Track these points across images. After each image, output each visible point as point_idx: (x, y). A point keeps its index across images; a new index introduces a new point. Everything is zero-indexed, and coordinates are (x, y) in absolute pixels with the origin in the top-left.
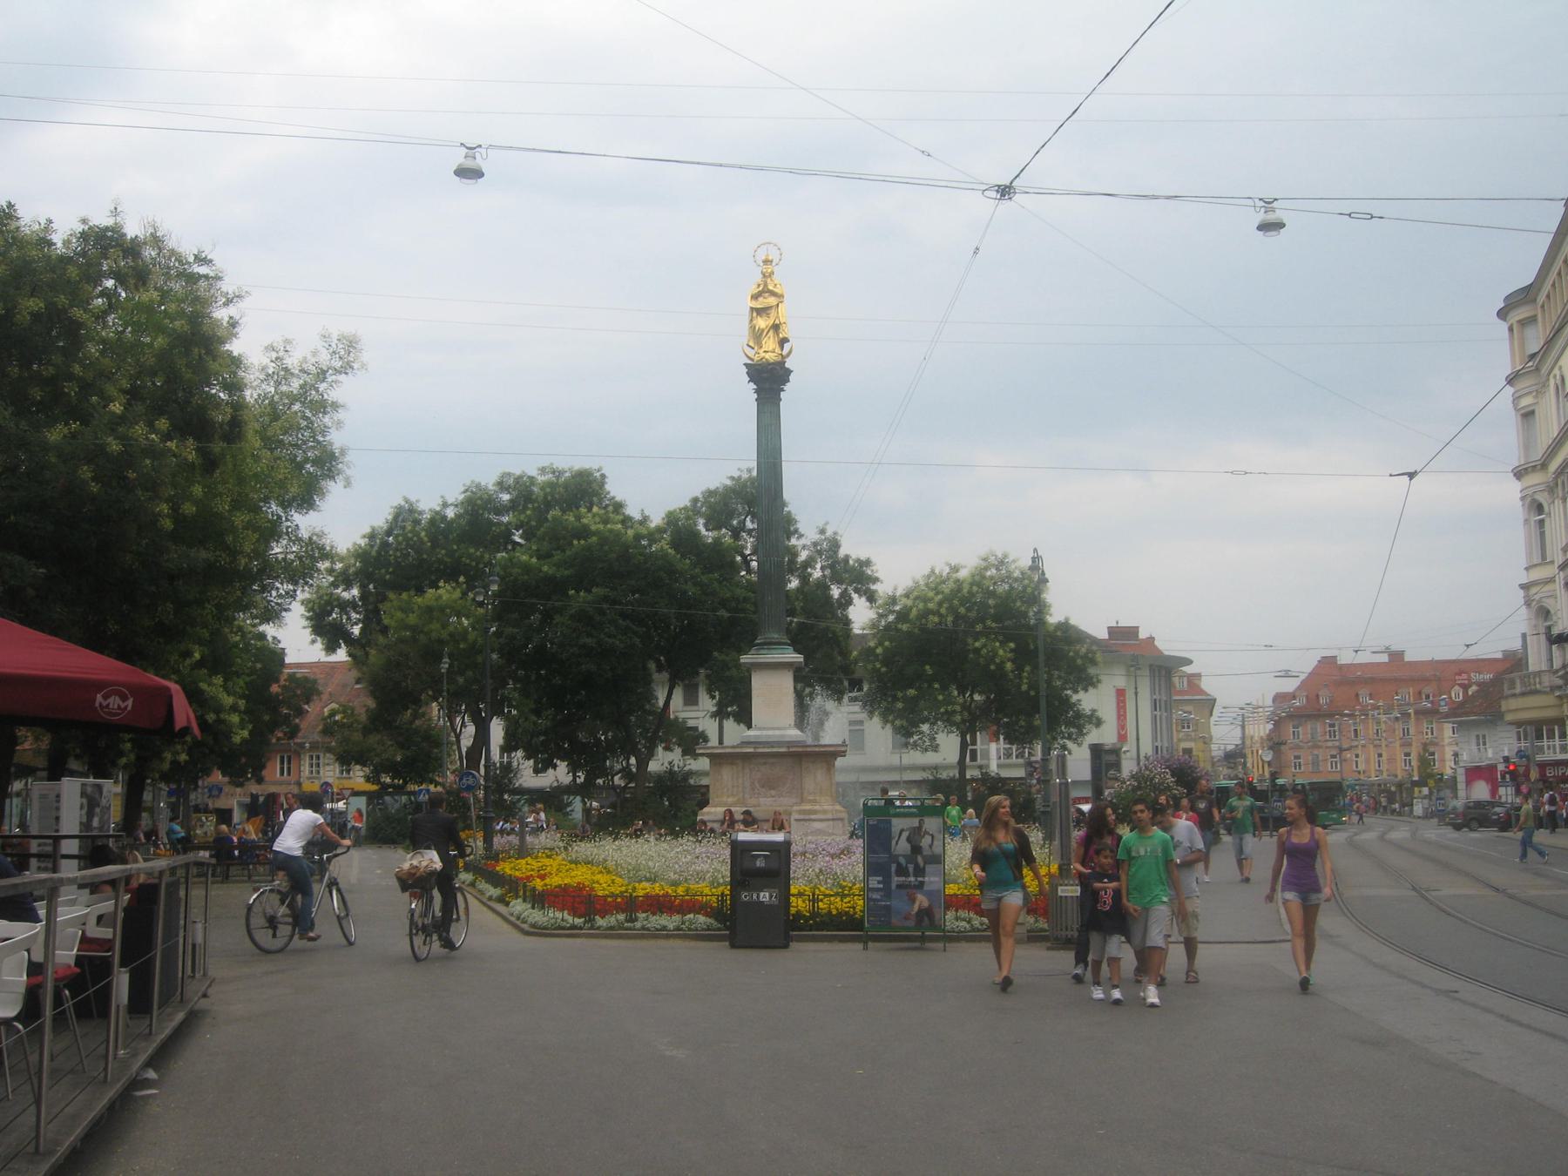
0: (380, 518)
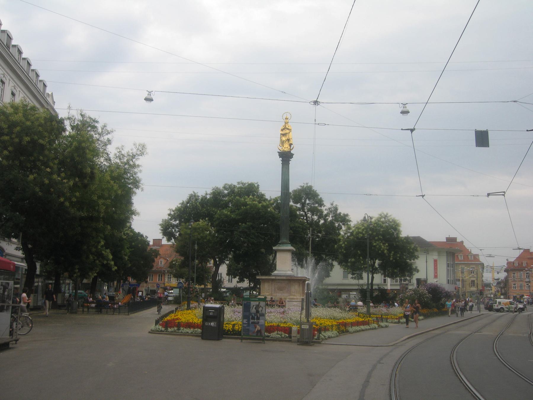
0: (185, 198)
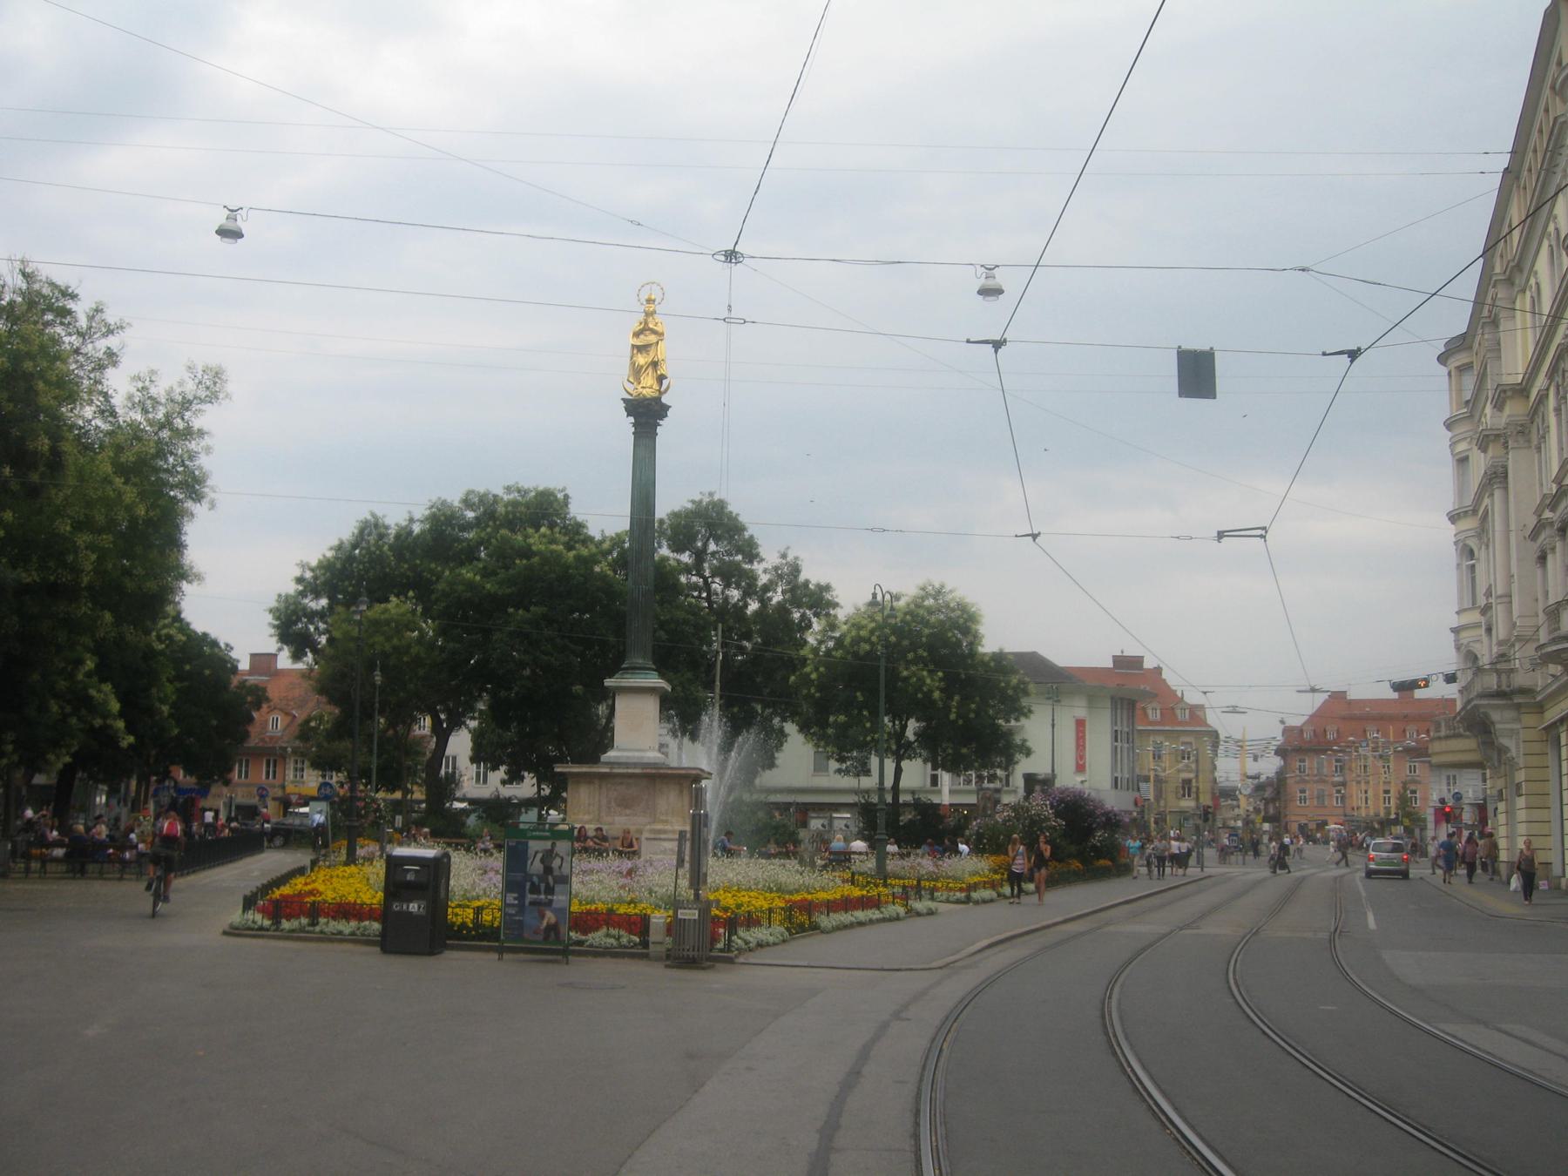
0: (345, 531)
